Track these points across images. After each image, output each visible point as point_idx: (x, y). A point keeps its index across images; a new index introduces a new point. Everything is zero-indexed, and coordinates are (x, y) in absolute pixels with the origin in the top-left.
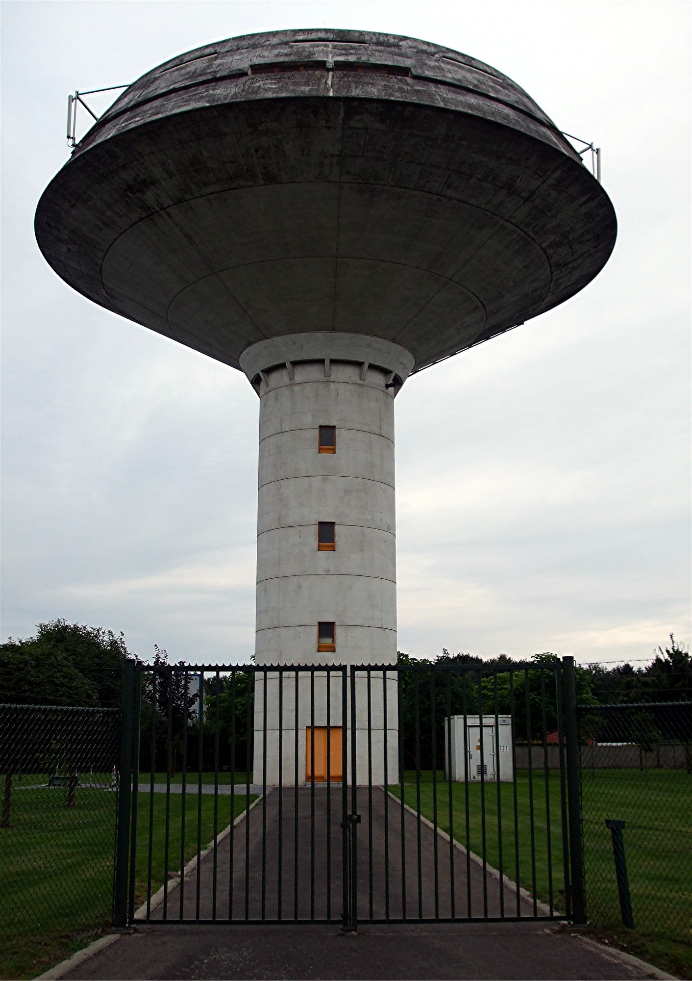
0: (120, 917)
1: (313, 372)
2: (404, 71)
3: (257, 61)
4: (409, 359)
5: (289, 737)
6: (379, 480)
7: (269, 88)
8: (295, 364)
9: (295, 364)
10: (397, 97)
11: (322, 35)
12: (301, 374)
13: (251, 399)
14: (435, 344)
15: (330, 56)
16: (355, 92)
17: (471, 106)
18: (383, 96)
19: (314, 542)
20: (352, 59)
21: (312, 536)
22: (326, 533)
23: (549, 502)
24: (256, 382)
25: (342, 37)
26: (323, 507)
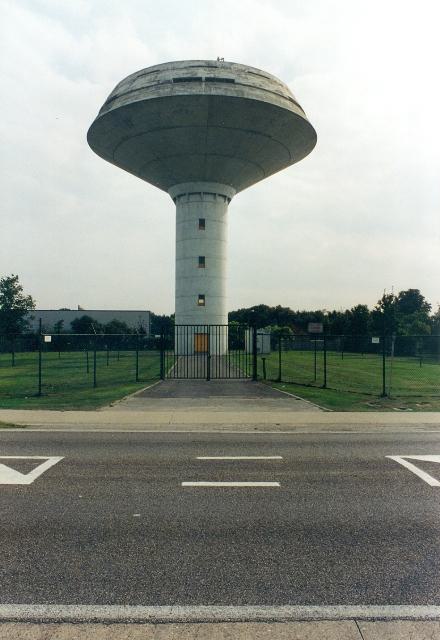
0: (162, 378)
1: (197, 197)
2: (232, 81)
3: (176, 77)
4: (235, 191)
5: (189, 336)
6: (218, 239)
7: (181, 91)
8: (190, 194)
9: (190, 194)
10: (229, 94)
11: (200, 64)
12: (192, 198)
13: (173, 207)
14: (240, 184)
15: (203, 73)
16: (213, 92)
17: (257, 96)
18: (224, 94)
19: (197, 265)
20: (212, 76)
21: (197, 261)
22: (202, 297)
23: (287, 243)
24: (174, 200)
25: (209, 65)
26: (197, 256)
